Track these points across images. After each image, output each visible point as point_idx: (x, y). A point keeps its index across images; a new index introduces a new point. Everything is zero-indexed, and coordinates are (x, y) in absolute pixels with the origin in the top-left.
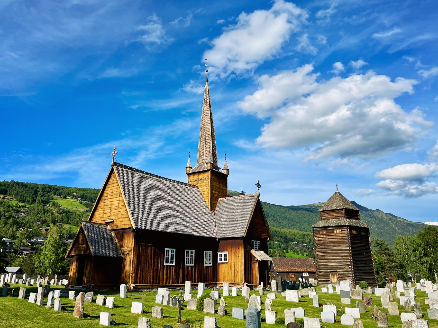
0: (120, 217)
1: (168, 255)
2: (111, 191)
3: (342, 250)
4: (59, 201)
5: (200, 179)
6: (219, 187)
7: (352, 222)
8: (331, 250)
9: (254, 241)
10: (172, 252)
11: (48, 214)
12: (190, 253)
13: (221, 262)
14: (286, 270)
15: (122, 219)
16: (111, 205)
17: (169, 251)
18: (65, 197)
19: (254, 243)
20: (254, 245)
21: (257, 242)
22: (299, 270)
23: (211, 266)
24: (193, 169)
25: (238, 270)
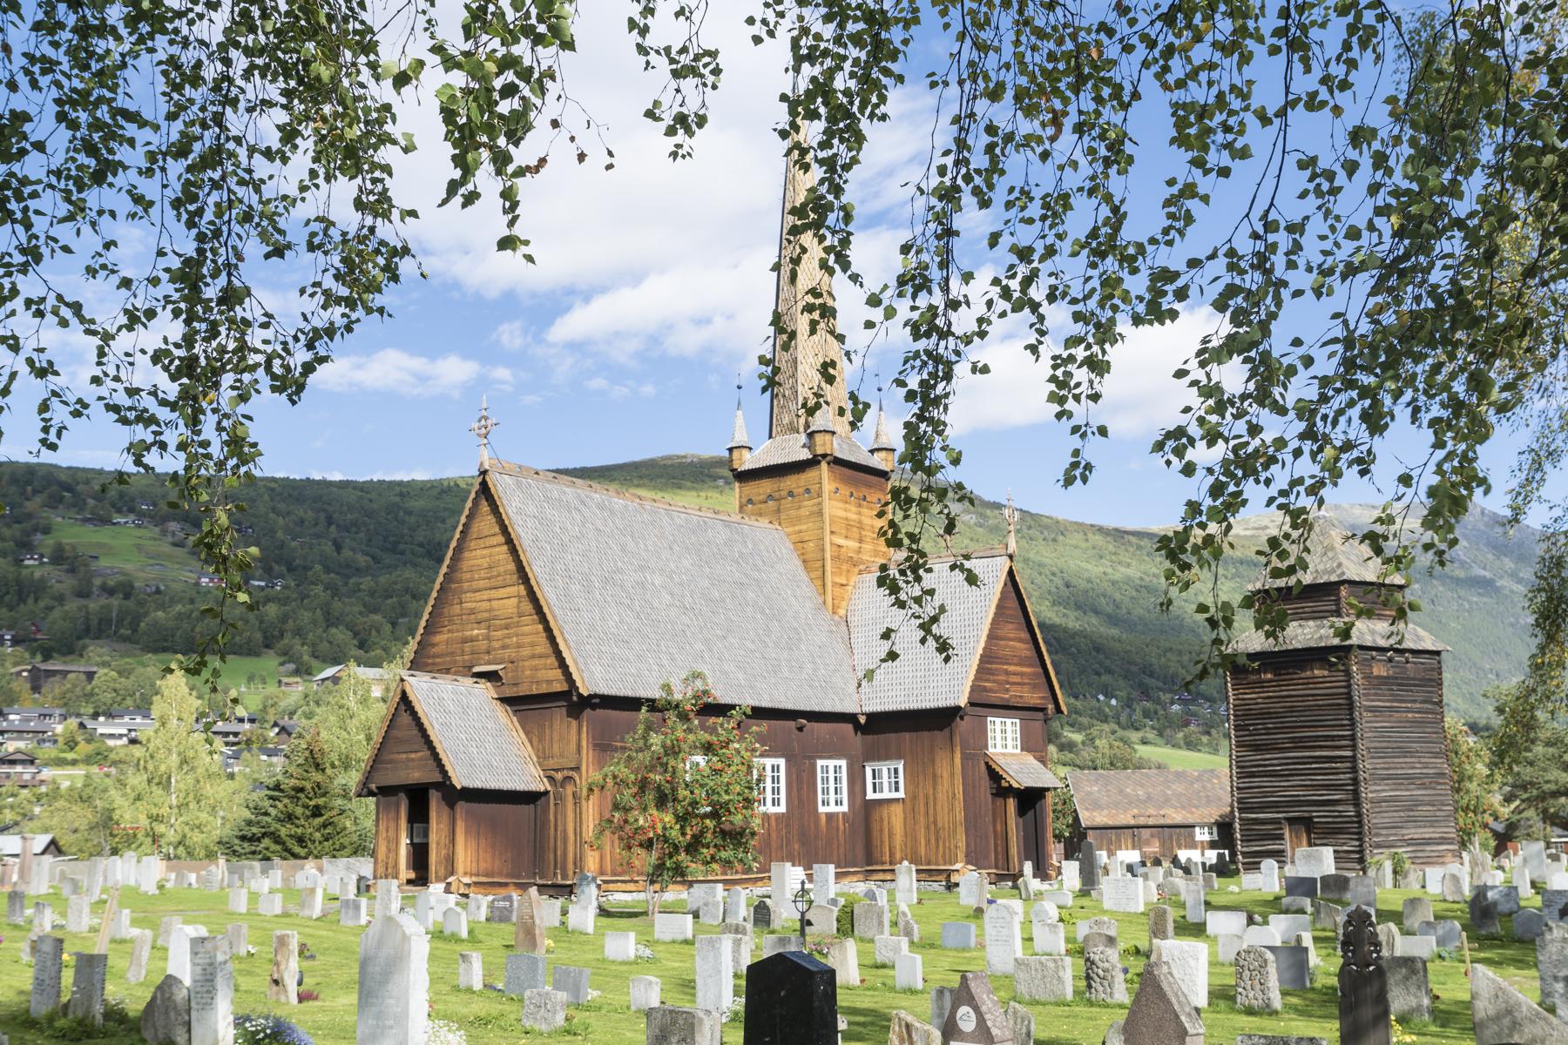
0: (526, 652)
1: (826, 780)
2: (485, 562)
3: (1332, 738)
4: (72, 533)
5: (784, 493)
6: (860, 522)
7: (1373, 632)
8: (1293, 740)
9: (998, 720)
10: (775, 768)
11: (42, 604)
12: (831, 771)
13: (878, 796)
14: (1125, 819)
15: (536, 662)
16: (490, 611)
17: (880, 771)
18: (106, 521)
19: (998, 727)
20: (998, 735)
21: (1009, 721)
22: (1178, 818)
23: (844, 814)
24: (756, 452)
25: (940, 824)
